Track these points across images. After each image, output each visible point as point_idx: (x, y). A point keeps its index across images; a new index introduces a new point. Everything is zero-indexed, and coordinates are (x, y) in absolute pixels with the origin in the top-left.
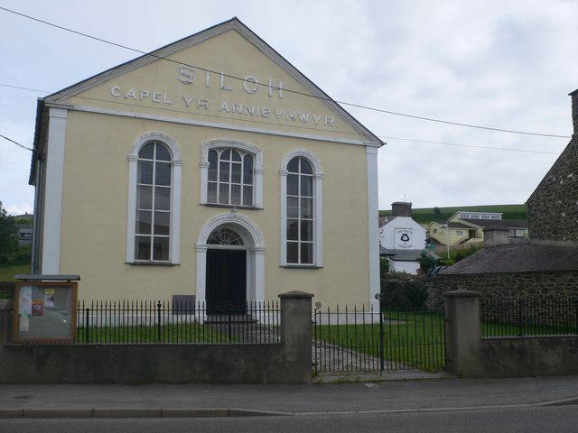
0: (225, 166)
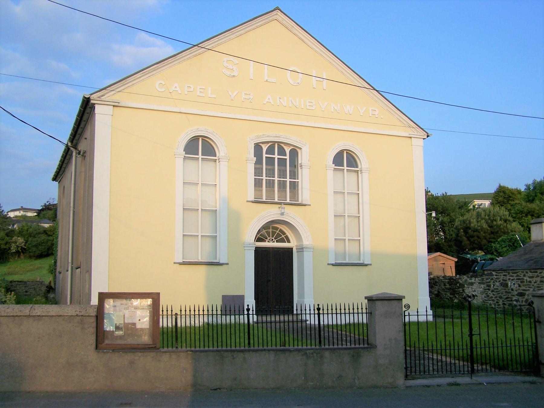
0: (270, 161)
